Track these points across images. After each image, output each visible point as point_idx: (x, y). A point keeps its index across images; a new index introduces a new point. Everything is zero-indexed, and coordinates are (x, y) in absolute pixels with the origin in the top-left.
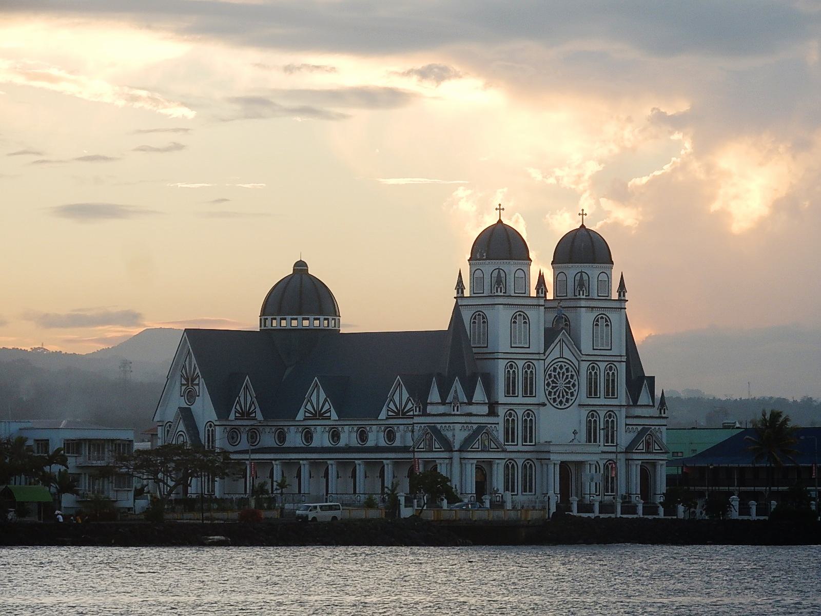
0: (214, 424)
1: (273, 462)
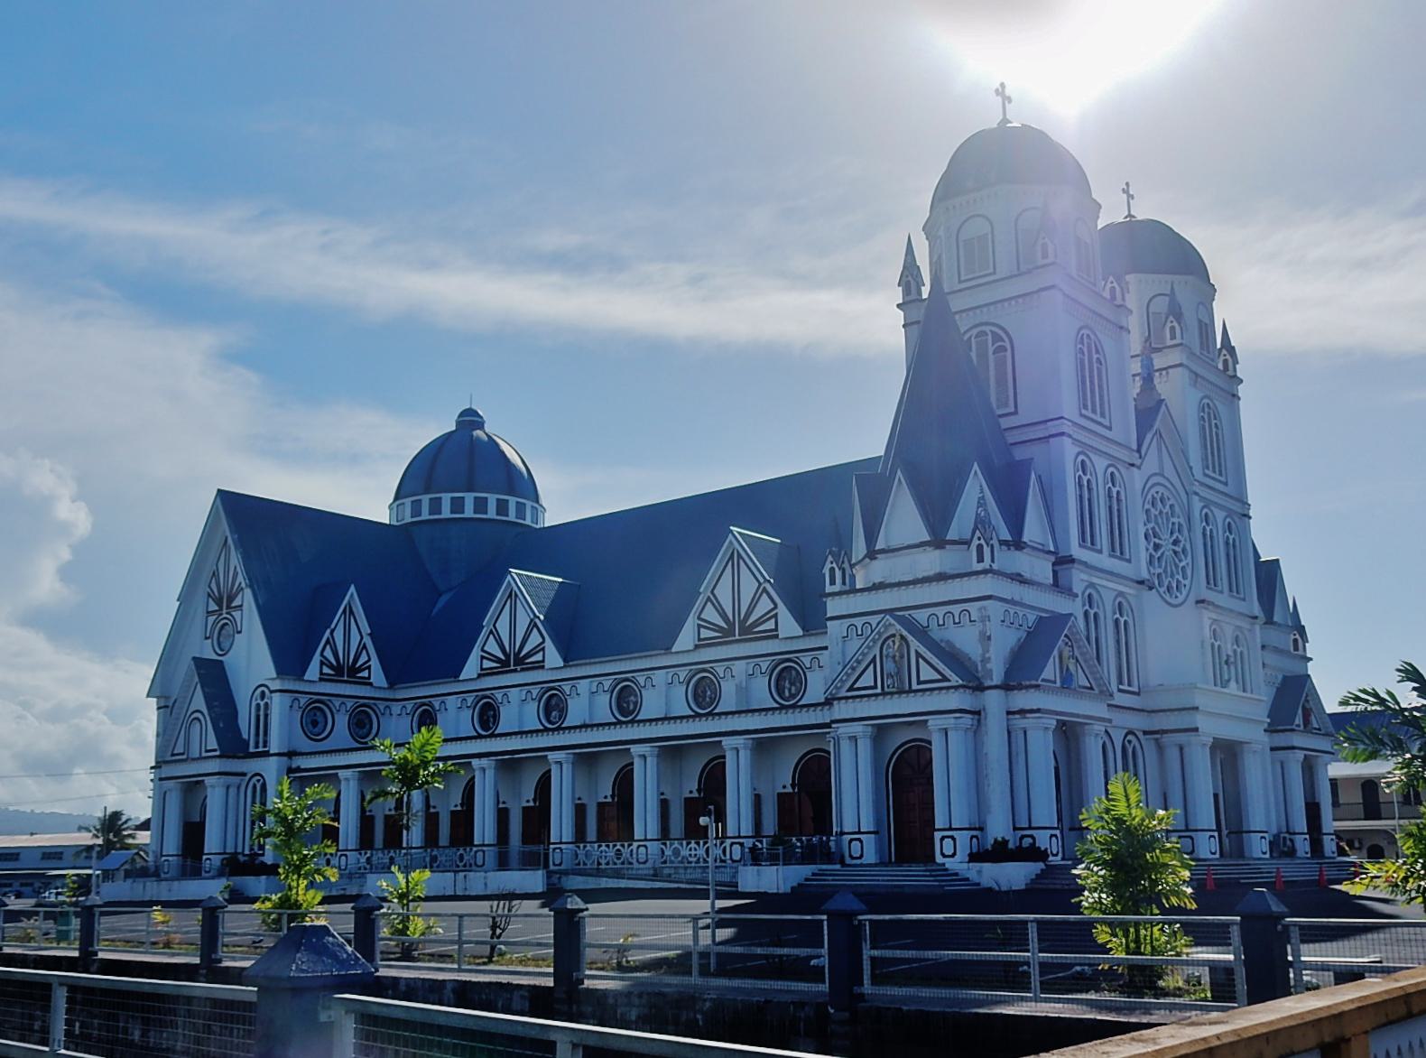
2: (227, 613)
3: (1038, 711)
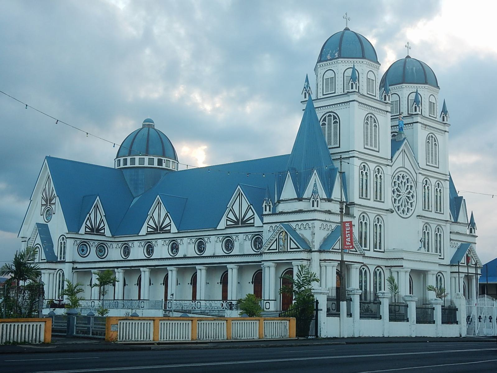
0: (65, 237)
1: (116, 270)
2: (49, 206)
3: (330, 260)
